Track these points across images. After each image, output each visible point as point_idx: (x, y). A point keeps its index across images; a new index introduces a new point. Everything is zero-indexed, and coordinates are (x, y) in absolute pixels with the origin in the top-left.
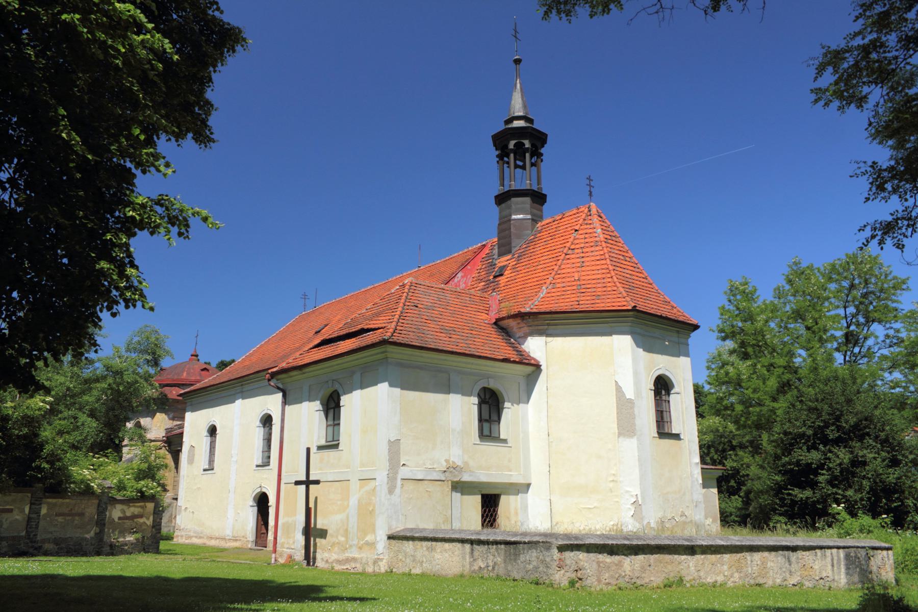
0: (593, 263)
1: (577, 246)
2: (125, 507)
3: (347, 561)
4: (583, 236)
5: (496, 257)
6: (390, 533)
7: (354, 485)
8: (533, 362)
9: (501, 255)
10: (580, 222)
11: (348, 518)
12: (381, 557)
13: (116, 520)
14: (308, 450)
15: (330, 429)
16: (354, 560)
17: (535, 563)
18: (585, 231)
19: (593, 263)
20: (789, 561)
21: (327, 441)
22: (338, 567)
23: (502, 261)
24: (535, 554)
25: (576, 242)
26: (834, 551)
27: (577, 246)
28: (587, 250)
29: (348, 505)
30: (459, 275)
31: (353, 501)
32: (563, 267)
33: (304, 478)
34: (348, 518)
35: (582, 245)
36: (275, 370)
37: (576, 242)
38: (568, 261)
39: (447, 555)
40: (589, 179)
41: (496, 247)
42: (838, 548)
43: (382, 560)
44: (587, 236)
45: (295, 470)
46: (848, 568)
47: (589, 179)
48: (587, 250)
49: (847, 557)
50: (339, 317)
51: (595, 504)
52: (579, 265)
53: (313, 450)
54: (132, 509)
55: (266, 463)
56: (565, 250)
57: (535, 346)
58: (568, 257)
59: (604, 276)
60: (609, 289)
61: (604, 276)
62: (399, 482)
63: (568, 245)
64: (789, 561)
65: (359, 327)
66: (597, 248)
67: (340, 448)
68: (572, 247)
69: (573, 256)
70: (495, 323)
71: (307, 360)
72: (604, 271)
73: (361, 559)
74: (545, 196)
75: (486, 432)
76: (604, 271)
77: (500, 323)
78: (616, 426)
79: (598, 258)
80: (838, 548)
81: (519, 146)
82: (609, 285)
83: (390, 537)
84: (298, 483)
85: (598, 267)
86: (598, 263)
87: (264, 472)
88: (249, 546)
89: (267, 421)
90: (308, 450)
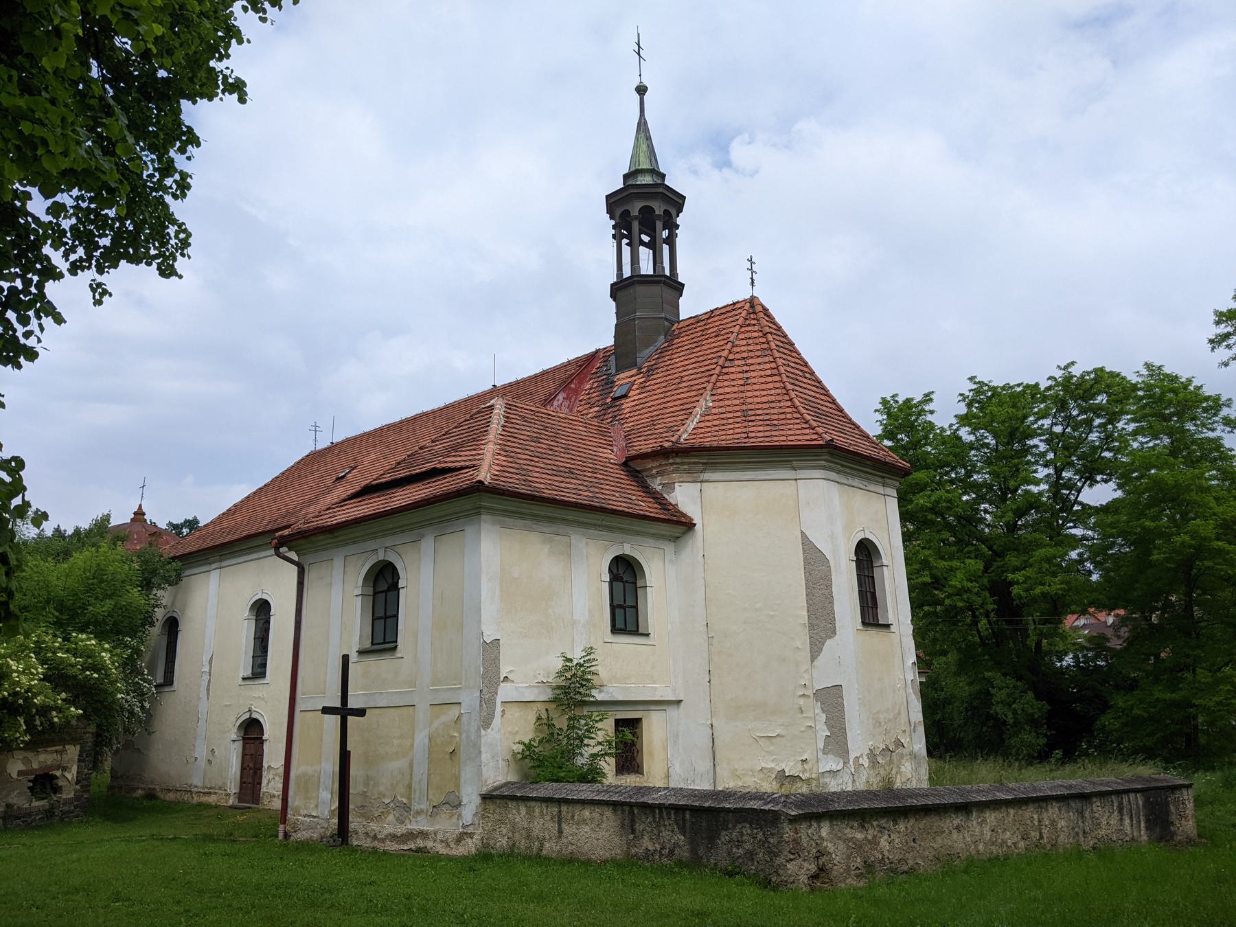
0: (762, 380)
1: (738, 356)
2: (30, 755)
3: (411, 836)
4: (744, 342)
5: (613, 371)
6: (484, 790)
7: (423, 712)
8: (683, 519)
9: (620, 370)
10: (740, 322)
11: (411, 766)
12: (470, 830)
13: (15, 775)
14: (345, 659)
15: (380, 623)
16: (423, 834)
17: (748, 846)
18: (747, 335)
19: (762, 380)
20: (1083, 817)
21: (372, 644)
22: (392, 846)
23: (623, 378)
24: (747, 831)
25: (735, 349)
26: (1132, 796)
27: (738, 356)
28: (750, 361)
29: (412, 745)
30: (561, 397)
31: (421, 738)
32: (719, 384)
33: (337, 703)
34: (411, 766)
35: (745, 355)
36: (286, 532)
37: (735, 349)
38: (726, 377)
39: (587, 828)
40: (750, 260)
41: (613, 358)
42: (1136, 791)
43: (471, 835)
44: (750, 342)
45: (321, 686)
46: (1148, 821)
47: (750, 260)
48: (750, 361)
49: (1147, 803)
50: (373, 456)
51: (778, 731)
52: (742, 382)
53: (353, 657)
54: (42, 757)
55: (259, 670)
56: (721, 362)
57: (685, 496)
58: (725, 370)
59: (779, 398)
60: (789, 416)
61: (779, 398)
62: (499, 708)
63: (725, 353)
64: (1083, 817)
65: (428, 466)
66: (767, 359)
67: (398, 654)
68: (731, 357)
69: (732, 370)
70: (625, 464)
71: (341, 516)
72: (779, 391)
73: (436, 833)
74: (683, 285)
75: (620, 625)
76: (779, 391)
77: (630, 463)
78: (805, 613)
79: (769, 372)
80: (1136, 791)
81: (647, 212)
82: (787, 410)
83: (487, 798)
84: (326, 710)
85: (771, 386)
86: (770, 379)
87: (258, 690)
88: (231, 802)
89: (262, 609)
90: (345, 659)
